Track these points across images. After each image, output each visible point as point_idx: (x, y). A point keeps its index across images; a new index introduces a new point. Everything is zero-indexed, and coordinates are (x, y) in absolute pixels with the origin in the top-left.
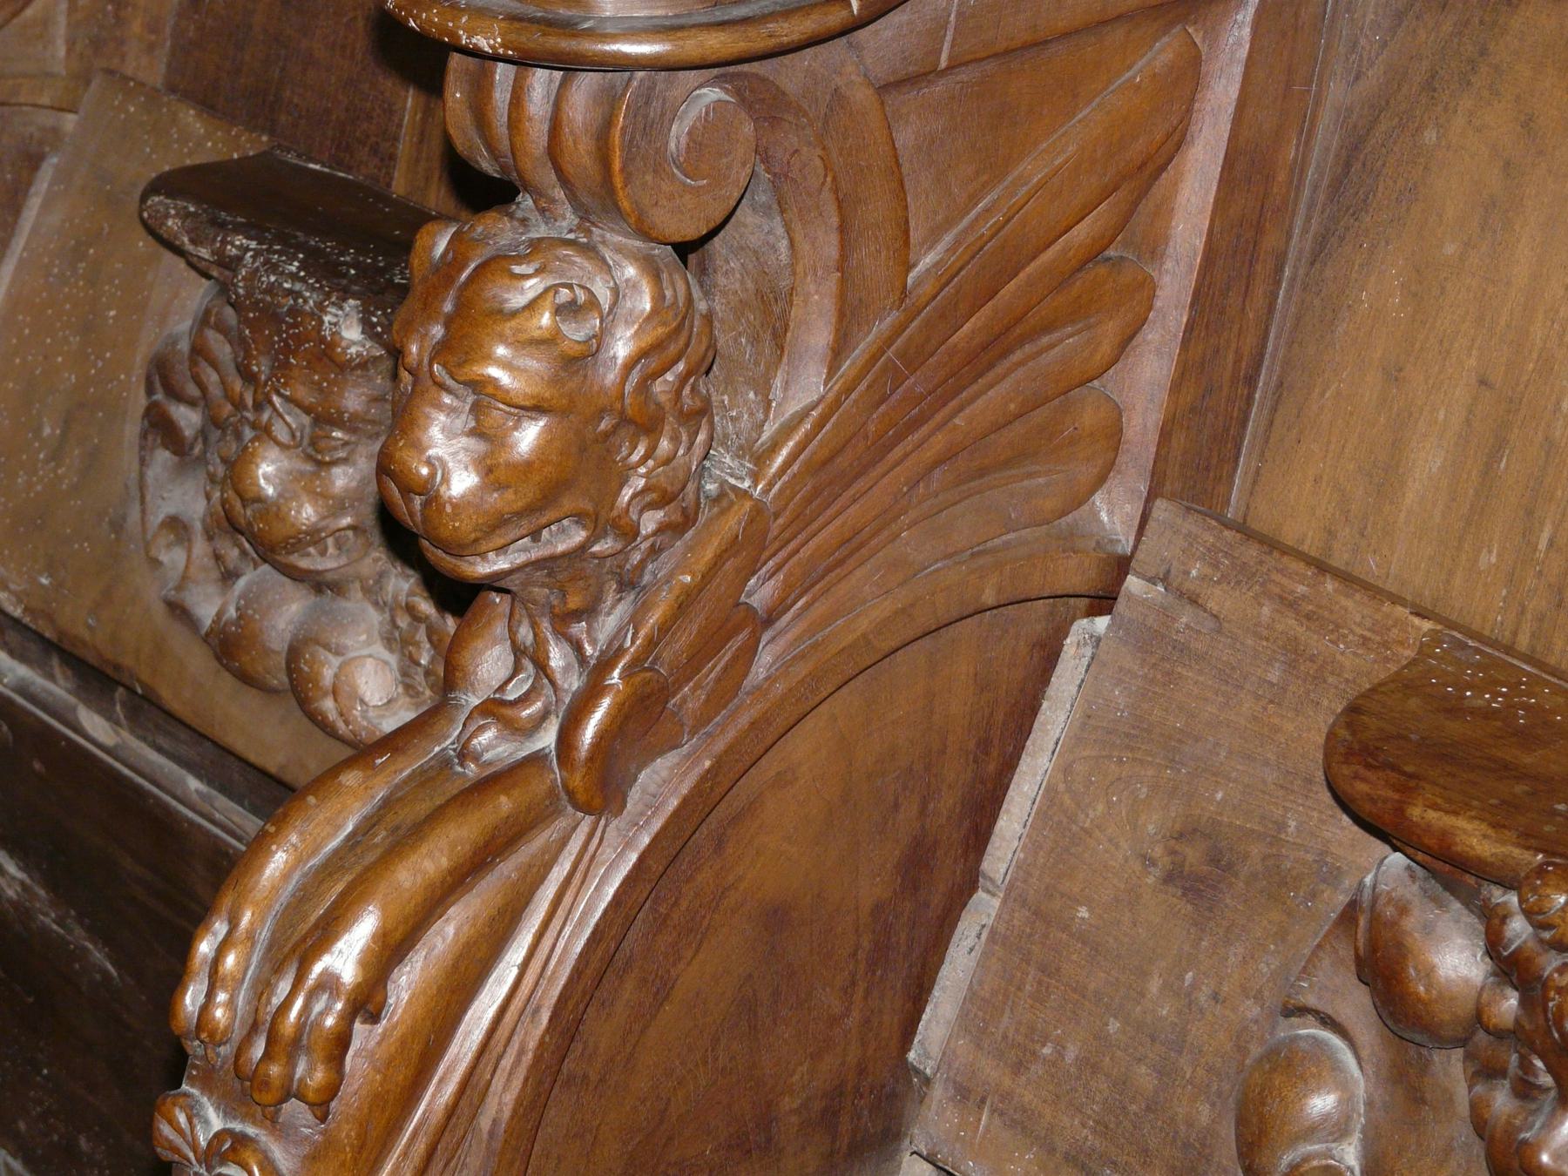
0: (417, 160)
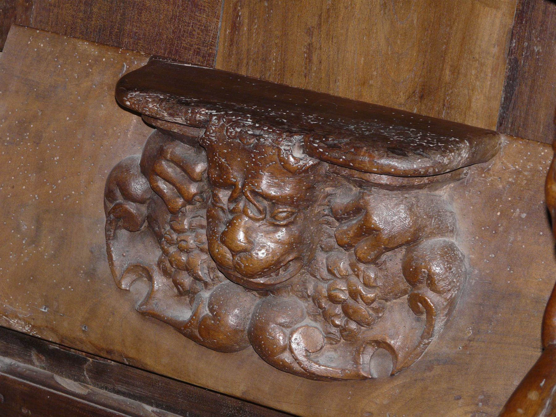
0: (230, 56)
